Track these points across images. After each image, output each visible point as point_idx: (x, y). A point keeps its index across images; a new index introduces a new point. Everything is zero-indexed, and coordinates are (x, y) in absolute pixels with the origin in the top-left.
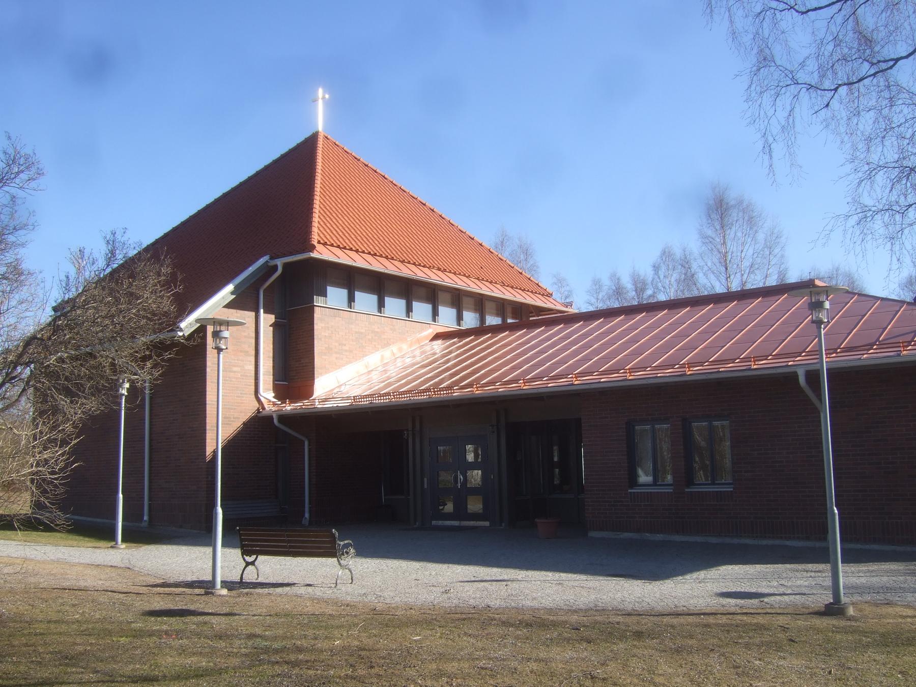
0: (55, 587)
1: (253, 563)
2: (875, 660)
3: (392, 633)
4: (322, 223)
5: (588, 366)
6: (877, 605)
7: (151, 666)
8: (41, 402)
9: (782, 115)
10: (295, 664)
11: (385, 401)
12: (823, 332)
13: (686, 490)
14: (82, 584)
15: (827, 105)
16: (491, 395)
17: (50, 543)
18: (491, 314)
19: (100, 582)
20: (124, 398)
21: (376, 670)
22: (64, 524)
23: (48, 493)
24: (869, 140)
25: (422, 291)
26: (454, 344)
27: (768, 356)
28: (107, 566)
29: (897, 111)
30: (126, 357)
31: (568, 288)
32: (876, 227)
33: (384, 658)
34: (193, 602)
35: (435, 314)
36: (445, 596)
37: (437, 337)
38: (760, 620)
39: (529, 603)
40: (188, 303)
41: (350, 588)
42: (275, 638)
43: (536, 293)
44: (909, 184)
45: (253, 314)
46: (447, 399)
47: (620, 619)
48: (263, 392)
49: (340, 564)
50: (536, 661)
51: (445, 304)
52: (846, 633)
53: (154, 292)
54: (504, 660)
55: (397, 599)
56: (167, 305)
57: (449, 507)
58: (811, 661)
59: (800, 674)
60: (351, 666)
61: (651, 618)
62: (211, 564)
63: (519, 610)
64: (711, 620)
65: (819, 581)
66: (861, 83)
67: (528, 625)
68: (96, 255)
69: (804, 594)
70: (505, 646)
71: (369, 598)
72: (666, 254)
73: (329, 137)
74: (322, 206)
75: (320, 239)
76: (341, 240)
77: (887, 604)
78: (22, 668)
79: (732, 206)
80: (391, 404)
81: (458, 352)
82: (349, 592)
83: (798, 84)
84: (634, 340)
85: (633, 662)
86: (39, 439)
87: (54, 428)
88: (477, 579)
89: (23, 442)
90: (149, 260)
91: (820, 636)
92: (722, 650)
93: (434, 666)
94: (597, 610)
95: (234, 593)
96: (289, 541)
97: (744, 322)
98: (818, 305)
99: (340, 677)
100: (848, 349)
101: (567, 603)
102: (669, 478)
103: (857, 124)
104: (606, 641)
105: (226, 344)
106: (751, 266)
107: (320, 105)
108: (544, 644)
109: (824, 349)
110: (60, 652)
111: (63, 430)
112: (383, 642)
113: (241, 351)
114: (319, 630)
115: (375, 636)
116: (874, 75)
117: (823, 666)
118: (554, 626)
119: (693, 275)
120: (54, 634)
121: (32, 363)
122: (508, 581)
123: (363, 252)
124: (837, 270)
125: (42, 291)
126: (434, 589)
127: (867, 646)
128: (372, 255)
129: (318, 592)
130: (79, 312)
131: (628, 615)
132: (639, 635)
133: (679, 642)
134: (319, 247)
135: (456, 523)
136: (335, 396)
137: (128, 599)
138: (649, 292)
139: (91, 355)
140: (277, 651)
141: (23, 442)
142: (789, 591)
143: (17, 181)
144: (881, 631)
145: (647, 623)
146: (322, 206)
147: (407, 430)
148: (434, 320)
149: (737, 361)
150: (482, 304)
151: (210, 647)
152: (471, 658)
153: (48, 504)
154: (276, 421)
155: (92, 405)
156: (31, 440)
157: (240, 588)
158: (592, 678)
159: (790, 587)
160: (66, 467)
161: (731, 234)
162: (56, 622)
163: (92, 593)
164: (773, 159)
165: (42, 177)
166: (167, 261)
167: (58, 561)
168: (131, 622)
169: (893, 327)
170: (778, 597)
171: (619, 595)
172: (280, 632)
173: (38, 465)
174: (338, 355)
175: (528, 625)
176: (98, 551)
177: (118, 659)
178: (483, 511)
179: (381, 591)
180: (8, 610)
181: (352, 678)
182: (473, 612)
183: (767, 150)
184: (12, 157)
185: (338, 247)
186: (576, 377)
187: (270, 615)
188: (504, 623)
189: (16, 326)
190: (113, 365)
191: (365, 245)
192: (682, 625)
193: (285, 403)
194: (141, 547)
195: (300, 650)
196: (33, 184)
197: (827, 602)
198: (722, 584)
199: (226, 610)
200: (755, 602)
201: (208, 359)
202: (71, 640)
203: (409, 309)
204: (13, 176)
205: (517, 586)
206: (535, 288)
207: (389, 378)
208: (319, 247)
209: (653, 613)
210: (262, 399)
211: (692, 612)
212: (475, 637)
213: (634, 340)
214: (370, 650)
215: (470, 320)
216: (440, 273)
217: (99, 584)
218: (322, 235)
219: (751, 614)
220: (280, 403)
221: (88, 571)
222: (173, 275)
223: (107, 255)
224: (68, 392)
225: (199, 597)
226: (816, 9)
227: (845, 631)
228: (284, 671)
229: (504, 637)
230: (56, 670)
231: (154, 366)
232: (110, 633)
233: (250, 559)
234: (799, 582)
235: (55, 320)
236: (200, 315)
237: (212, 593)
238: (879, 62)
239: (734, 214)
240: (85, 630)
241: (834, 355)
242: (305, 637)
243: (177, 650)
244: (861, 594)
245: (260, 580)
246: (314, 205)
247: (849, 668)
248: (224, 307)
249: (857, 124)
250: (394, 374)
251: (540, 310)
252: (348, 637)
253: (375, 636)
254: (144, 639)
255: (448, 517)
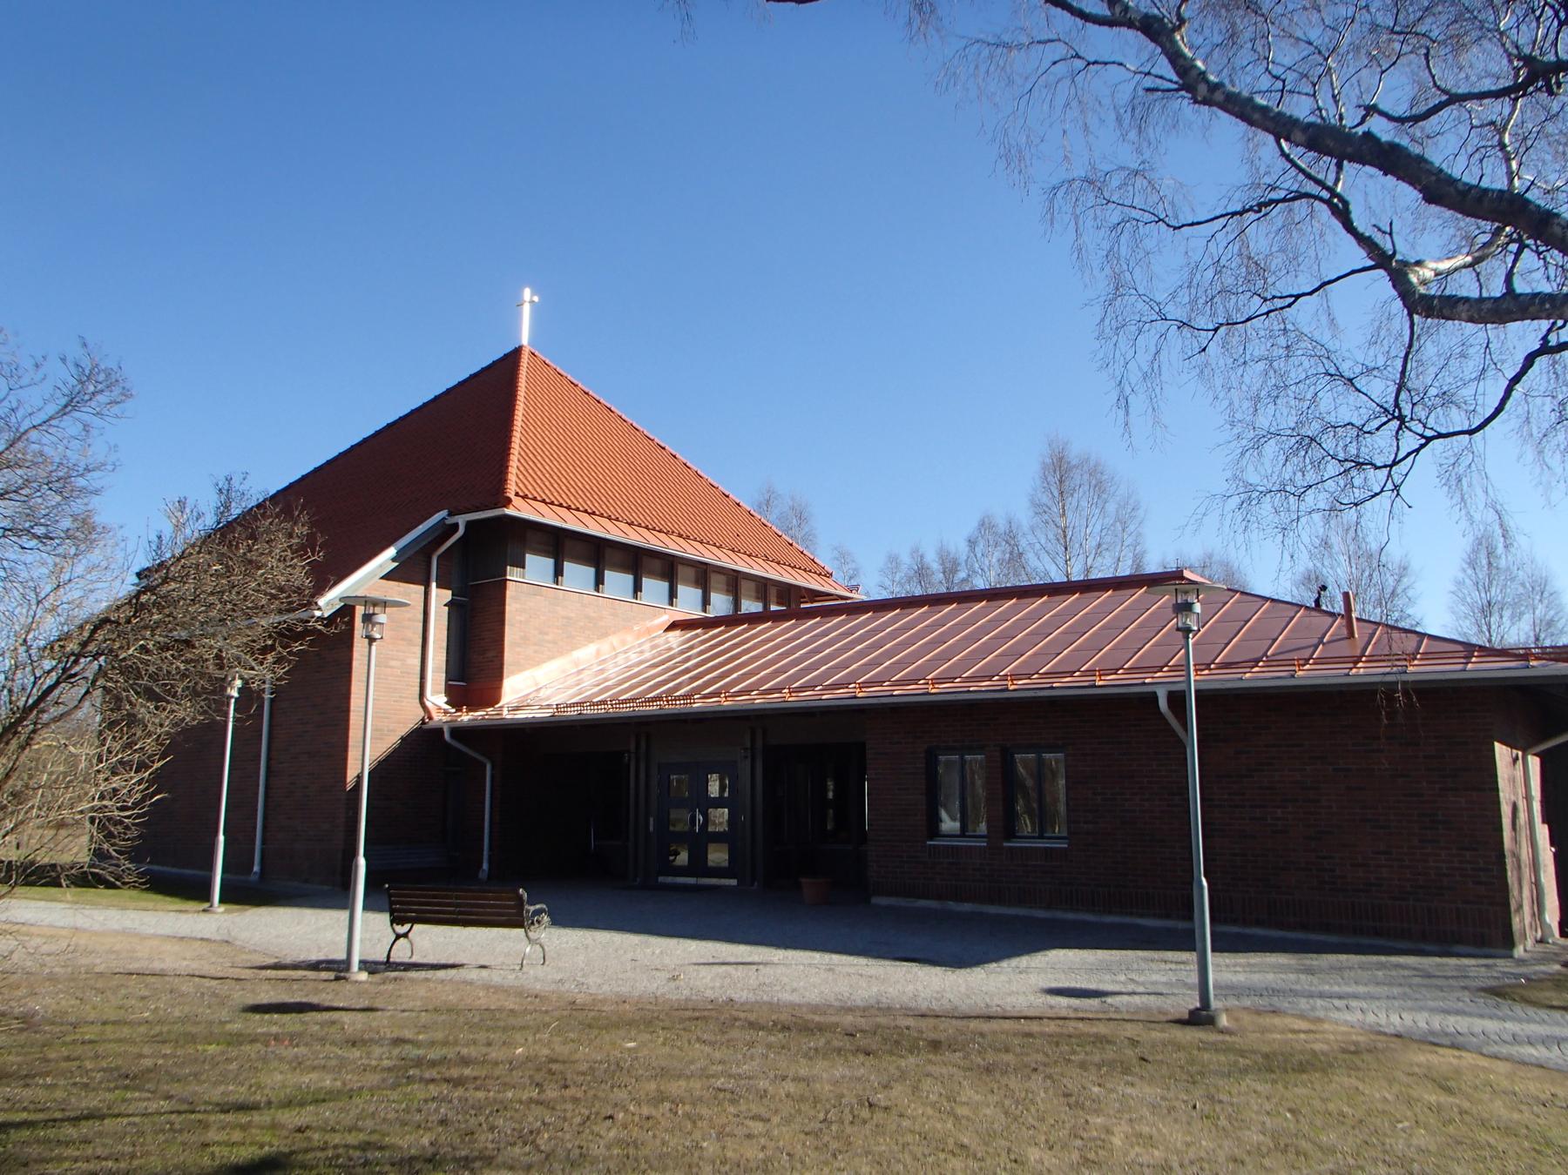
0: (117, 970)
1: (405, 935)
2: (1255, 1092)
3: (596, 1037)
4: (522, 469)
5: (877, 673)
6: (1258, 1013)
7: (251, 1086)
8: (112, 710)
9: (1143, 359)
10: (458, 1082)
11: (600, 711)
12: (1191, 641)
13: (1005, 844)
14: (157, 966)
15: (1204, 350)
16: (744, 708)
17: (114, 906)
18: (749, 597)
19: (185, 963)
20: (233, 701)
21: (568, 1093)
22: (135, 882)
23: (114, 837)
24: (1257, 399)
25: (657, 564)
26: (697, 636)
27: (1118, 670)
28: (195, 939)
29: (1296, 363)
30: (238, 647)
31: (854, 566)
32: (1264, 513)
33: (584, 1074)
34: (317, 991)
35: (672, 595)
36: (673, 985)
37: (673, 626)
38: (1101, 1029)
39: (786, 997)
40: (327, 576)
41: (540, 971)
42: (432, 1044)
43: (810, 571)
44: (1307, 461)
45: (422, 588)
46: (685, 711)
47: (910, 1022)
48: (432, 695)
49: (527, 936)
50: (794, 1080)
51: (686, 583)
52: (1216, 1050)
53: (282, 560)
54: (750, 1078)
55: (606, 988)
56: (299, 575)
57: (683, 858)
58: (1169, 1089)
59: (1154, 1107)
60: (537, 1085)
61: (954, 1022)
62: (345, 935)
63: (773, 1007)
64: (1035, 1027)
65: (1183, 976)
66: (1249, 323)
67: (786, 1028)
68: (203, 508)
69: (1161, 994)
70: (752, 1058)
71: (567, 986)
72: (985, 525)
73: (536, 353)
74: (523, 446)
75: (518, 490)
76: (547, 492)
77: (1274, 1012)
78: (59, 1094)
79: (1075, 466)
80: (608, 716)
81: (702, 647)
82: (539, 978)
83: (1166, 319)
84: (941, 640)
85: (927, 1084)
86: (107, 760)
87: (129, 745)
88: (717, 961)
89: (82, 765)
90: (278, 516)
91: (1182, 1055)
92: (1048, 1071)
93: (653, 1086)
94: (879, 1009)
95: (377, 977)
96: (457, 905)
97: (1088, 623)
98: (1186, 607)
99: (521, 1102)
100: (1226, 665)
101: (840, 997)
102: (983, 828)
103: (1242, 376)
104: (891, 1053)
105: (381, 632)
106: (1099, 545)
107: (526, 309)
108: (806, 1056)
109: (1192, 663)
110: (117, 1068)
111: (142, 749)
112: (584, 1050)
113: (403, 639)
114: (494, 1032)
115: (573, 1041)
116: (1267, 313)
117: (1185, 1098)
118: (820, 1030)
119: (1021, 554)
120: (110, 1041)
121: (101, 655)
122: (759, 964)
123: (578, 509)
124: (1210, 556)
125: (122, 554)
126: (658, 974)
127: (1245, 1071)
128: (589, 514)
129: (495, 977)
130: (173, 585)
131: (922, 1016)
132: (935, 1045)
133: (991, 1057)
134: (516, 501)
135: (691, 880)
136: (531, 703)
137: (222, 988)
138: (962, 575)
139: (188, 644)
140: (433, 1064)
141: (82, 765)
142: (1141, 989)
143: (93, 404)
144: (1264, 1049)
145: (948, 1029)
146: (523, 446)
147: (629, 751)
148: (671, 604)
149: (1077, 674)
150: (737, 585)
151: (338, 1057)
152: (704, 1075)
153: (114, 853)
154: (447, 736)
155: (186, 712)
156: (95, 761)
157: (386, 970)
158: (871, 1105)
159: (1143, 984)
160: (143, 799)
161: (1071, 502)
162: (114, 1023)
163: (171, 979)
164: (1130, 416)
165: (128, 400)
166: (304, 518)
167: (124, 932)
168: (226, 1022)
169: (1286, 639)
170: (1126, 998)
171: (911, 987)
172: (439, 1036)
173: (102, 797)
174: (536, 648)
175: (786, 1028)
176: (183, 917)
177: (204, 1077)
178: (730, 863)
179: (583, 976)
180: (44, 1007)
181: (539, 1103)
182: (710, 1007)
183: (1123, 401)
184: (87, 372)
185: (543, 501)
186: (860, 688)
187: (426, 1011)
188: (753, 1026)
189: (81, 603)
190: (218, 657)
191: (580, 500)
192: (994, 1033)
193: (461, 710)
194: (246, 910)
195: (465, 1061)
196: (116, 409)
197: (1192, 1007)
198: (1050, 976)
199: (366, 1003)
200: (1094, 1003)
201: (355, 649)
202: (135, 1050)
203: (637, 588)
204: (87, 397)
205: (772, 972)
206: (810, 566)
207: (606, 680)
208: (516, 501)
209: (956, 1014)
210: (428, 704)
211: (1008, 1014)
212: (712, 1044)
213: (941, 640)
214: (564, 1062)
215: (720, 604)
216: (680, 541)
217: (184, 966)
218: (521, 485)
219: (1089, 1019)
220: (454, 710)
221: (168, 947)
222: (311, 537)
223: (219, 508)
224: (150, 695)
225: (326, 984)
226: (1192, 224)
227: (1216, 1048)
228: (442, 1093)
229: (751, 1044)
230: (109, 1096)
231: (279, 661)
232: (192, 1039)
233: (401, 929)
234: (1155, 977)
235: (138, 595)
236: (345, 591)
237: (344, 978)
238: (1274, 297)
239: (1077, 477)
240: (157, 1035)
241: (1206, 672)
242: (475, 1042)
243: (290, 1063)
244: (1238, 996)
245: (416, 959)
246: (513, 445)
247: (1220, 1102)
248: (382, 578)
249: (1242, 376)
250: (614, 675)
251: (815, 595)
252: (535, 1042)
253: (573, 1041)
254: (243, 1048)
255: (681, 871)
